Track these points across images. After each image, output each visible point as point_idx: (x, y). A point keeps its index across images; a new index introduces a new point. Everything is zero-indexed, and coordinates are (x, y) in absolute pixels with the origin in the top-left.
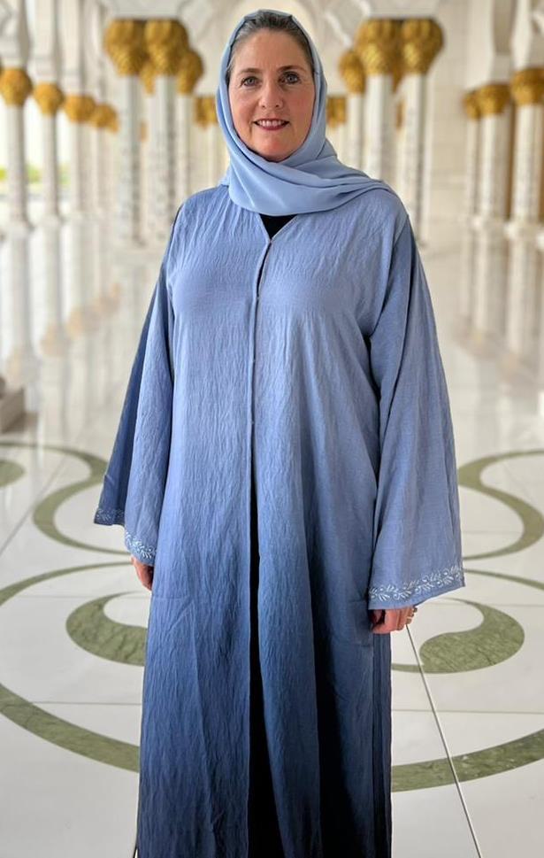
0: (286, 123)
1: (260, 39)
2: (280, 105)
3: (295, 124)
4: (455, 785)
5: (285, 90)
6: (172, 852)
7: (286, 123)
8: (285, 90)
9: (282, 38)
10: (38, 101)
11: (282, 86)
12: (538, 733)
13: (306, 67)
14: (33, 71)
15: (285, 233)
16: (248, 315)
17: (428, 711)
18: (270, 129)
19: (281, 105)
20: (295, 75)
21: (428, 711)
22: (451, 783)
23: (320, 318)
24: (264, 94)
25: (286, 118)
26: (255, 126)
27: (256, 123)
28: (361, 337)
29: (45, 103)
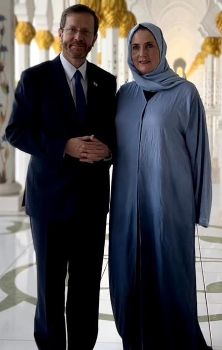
0: (149, 62)
1: (138, 34)
2: (146, 56)
3: (152, 62)
4: (208, 322)
5: (148, 50)
6: (142, 348)
7: (149, 62)
8: (148, 50)
9: (146, 32)
10: (38, 42)
11: (147, 49)
12: (31, 157)
13: (154, 41)
14: (35, 24)
15: (152, 100)
16: (139, 128)
17: (203, 303)
18: (144, 64)
19: (146, 55)
20: (151, 45)
21: (203, 303)
22: (206, 321)
23: (173, 70)
24: (141, 53)
25: (148, 60)
26: (139, 63)
27: (140, 62)
28: (181, 136)
29: (42, 42)
